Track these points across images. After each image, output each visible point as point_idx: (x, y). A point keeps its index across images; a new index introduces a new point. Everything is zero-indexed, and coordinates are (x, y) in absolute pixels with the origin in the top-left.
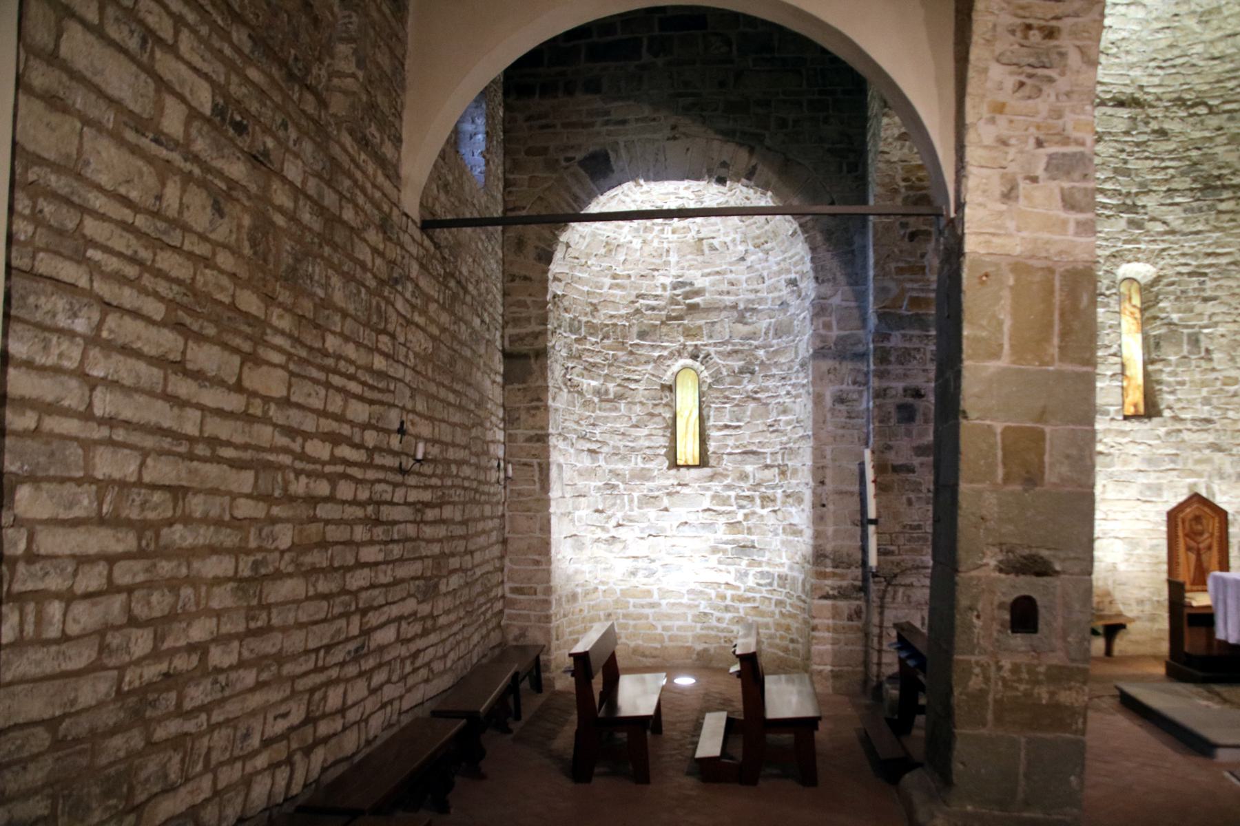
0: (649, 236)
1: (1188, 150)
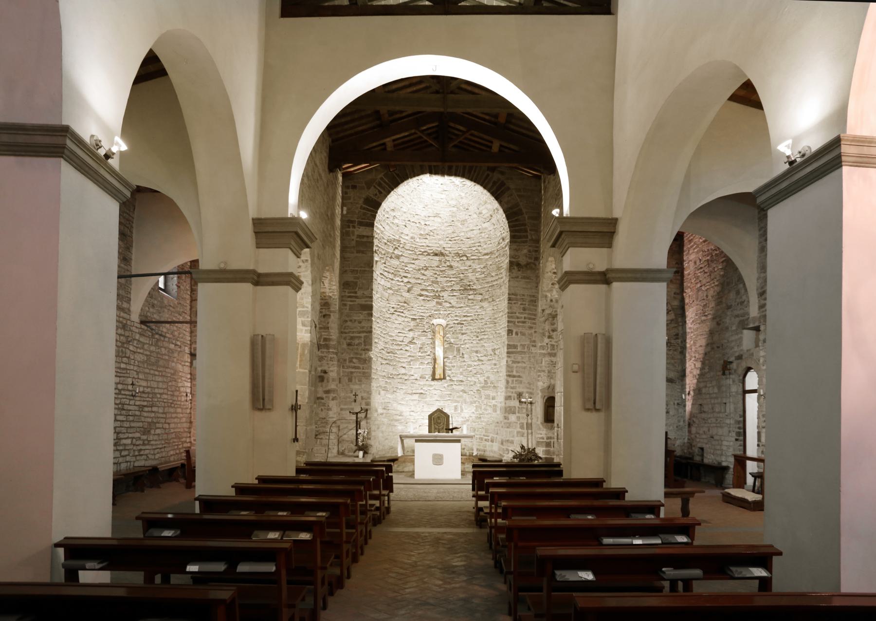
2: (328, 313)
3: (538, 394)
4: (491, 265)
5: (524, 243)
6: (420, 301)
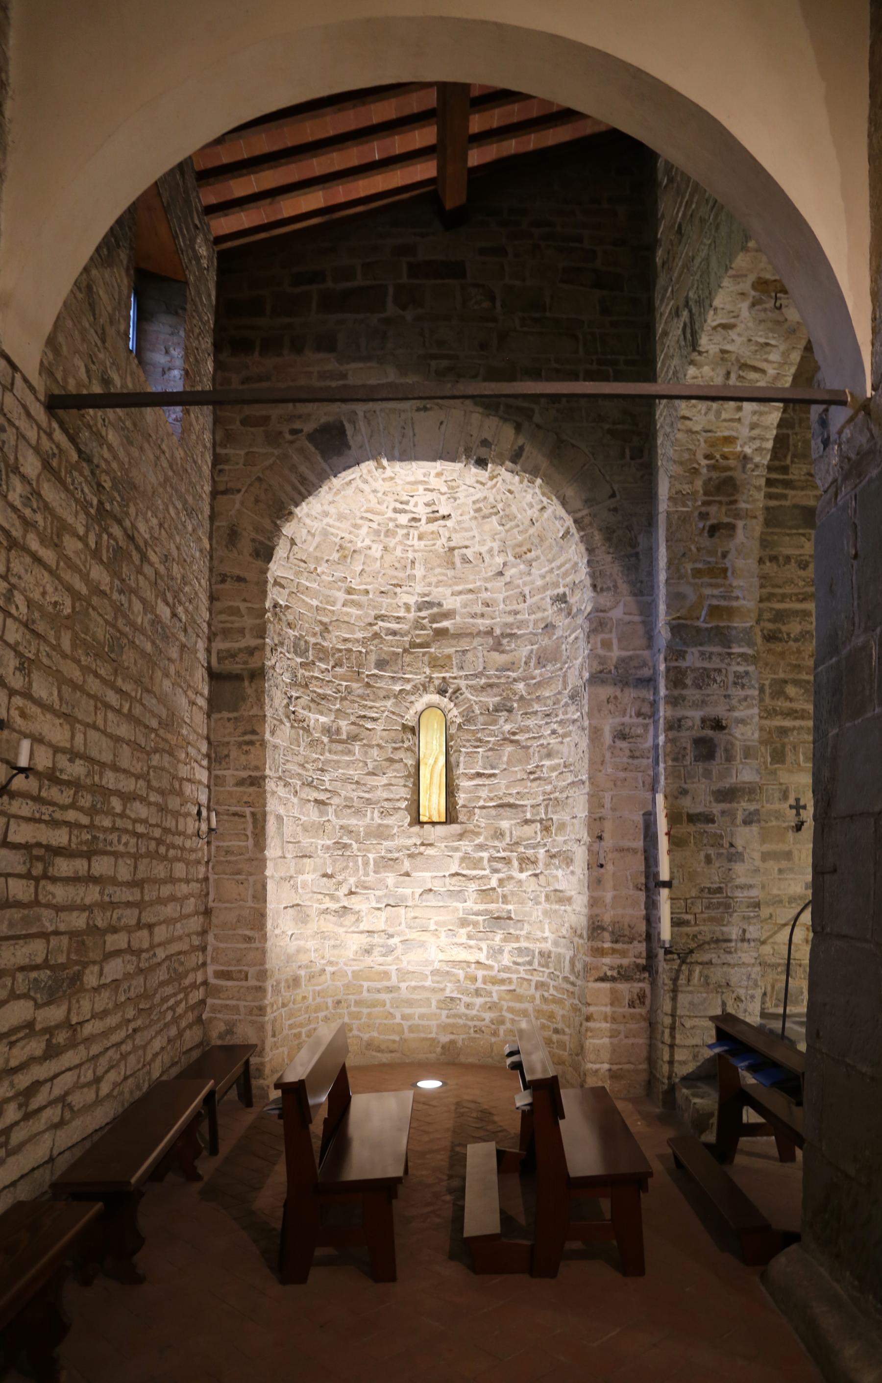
0: (392, 542)
2: (726, 520)
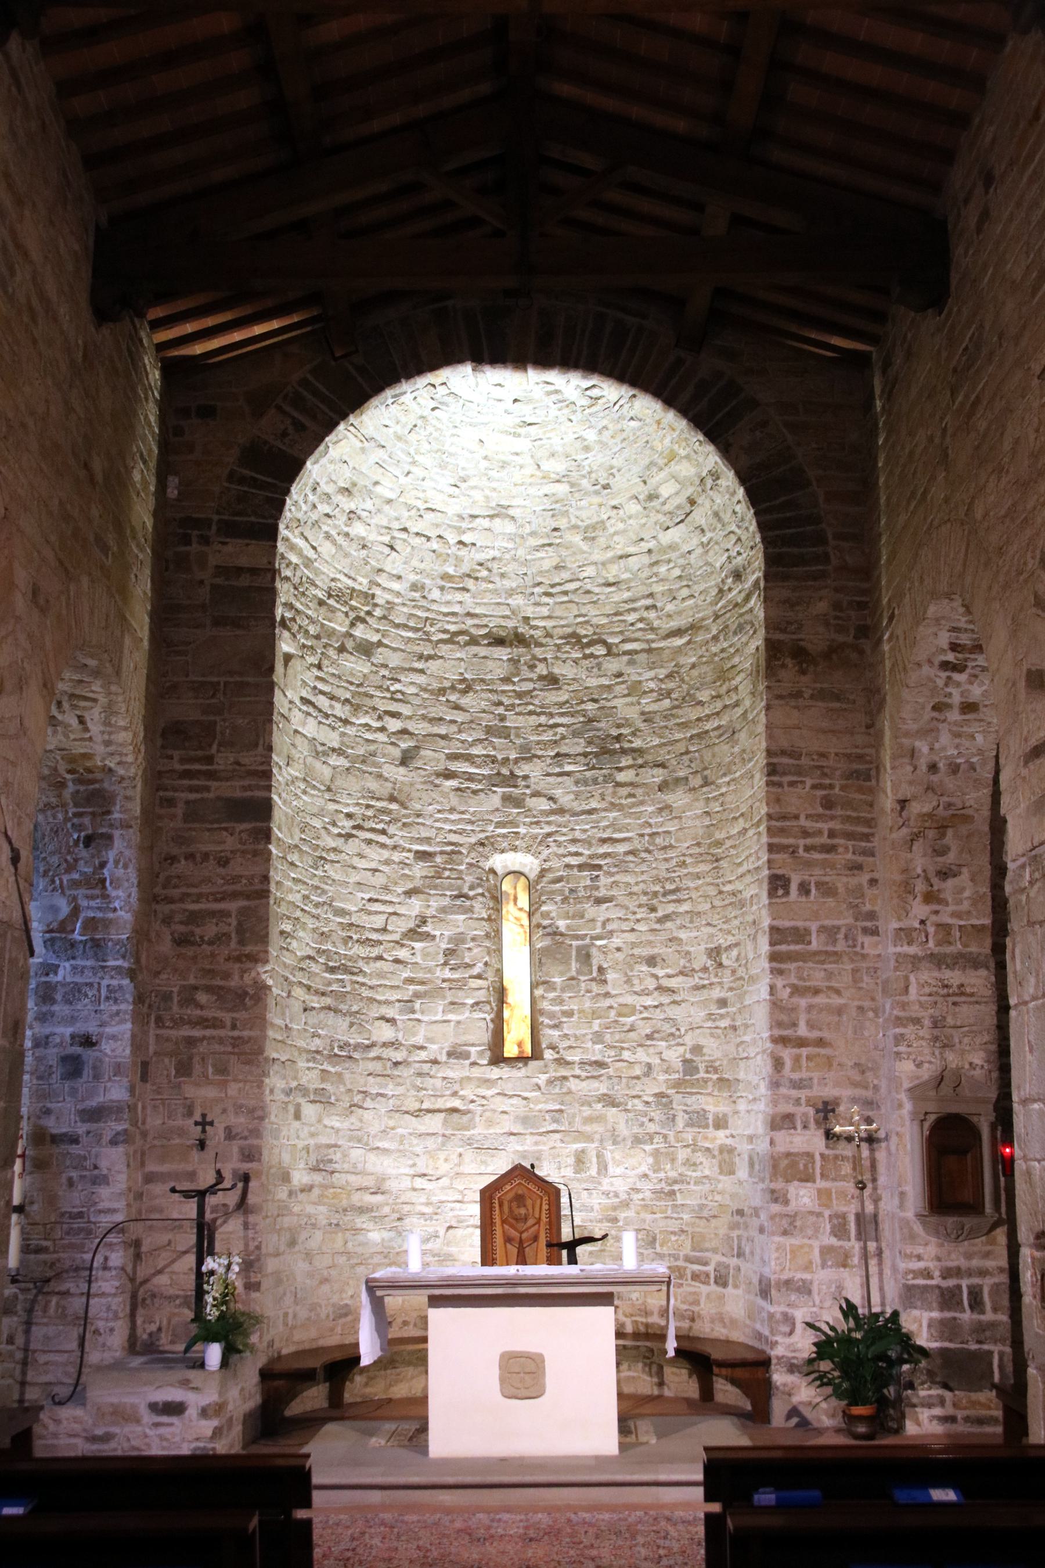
1: (583, 702)
3: (900, 1106)
4: (693, 666)
5: (815, 579)
6: (445, 795)
